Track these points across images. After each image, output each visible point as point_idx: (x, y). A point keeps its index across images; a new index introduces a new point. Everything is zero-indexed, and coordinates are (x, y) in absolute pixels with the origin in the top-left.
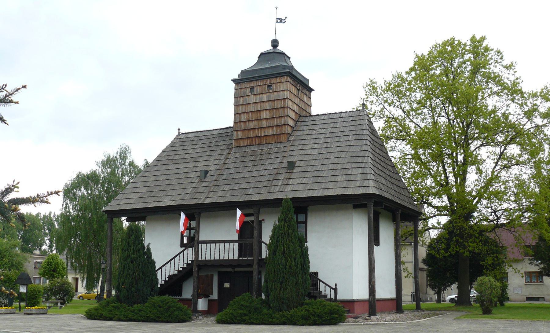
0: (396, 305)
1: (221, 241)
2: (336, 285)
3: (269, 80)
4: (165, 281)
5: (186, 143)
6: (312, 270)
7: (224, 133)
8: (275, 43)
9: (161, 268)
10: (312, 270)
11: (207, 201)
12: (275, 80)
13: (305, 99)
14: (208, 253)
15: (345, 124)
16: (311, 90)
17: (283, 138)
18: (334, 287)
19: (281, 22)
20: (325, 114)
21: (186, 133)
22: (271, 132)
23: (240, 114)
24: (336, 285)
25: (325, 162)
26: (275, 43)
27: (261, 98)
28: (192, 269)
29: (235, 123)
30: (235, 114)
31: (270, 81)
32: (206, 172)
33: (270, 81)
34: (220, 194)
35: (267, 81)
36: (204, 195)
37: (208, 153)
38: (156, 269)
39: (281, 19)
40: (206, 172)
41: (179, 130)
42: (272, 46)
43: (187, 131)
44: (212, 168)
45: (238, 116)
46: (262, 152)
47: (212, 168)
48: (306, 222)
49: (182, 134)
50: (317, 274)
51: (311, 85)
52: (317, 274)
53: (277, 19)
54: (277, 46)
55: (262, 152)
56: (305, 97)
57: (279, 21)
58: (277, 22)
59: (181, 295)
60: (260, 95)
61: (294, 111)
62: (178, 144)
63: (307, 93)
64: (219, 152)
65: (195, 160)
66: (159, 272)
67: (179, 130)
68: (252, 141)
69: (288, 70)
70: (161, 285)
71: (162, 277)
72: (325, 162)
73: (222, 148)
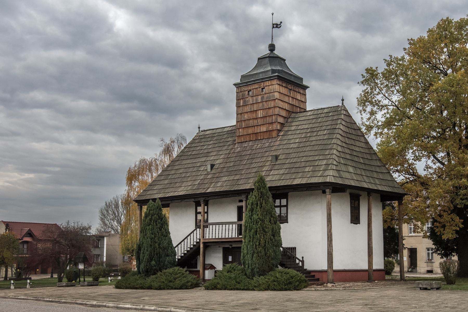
0: (368, 276)
1: (224, 222)
2: (303, 258)
3: (262, 84)
4: (181, 256)
5: (203, 140)
6: (285, 244)
7: (232, 132)
8: (272, 47)
9: (177, 246)
10: (285, 244)
11: (209, 191)
12: (267, 83)
13: (299, 97)
14: (213, 233)
15: (325, 119)
16: (305, 88)
17: (274, 134)
18: (301, 259)
19: (277, 27)
20: (312, 110)
21: (204, 131)
22: (264, 129)
23: (241, 114)
24: (303, 258)
25: (302, 154)
26: (272, 47)
27: (257, 100)
28: (200, 246)
29: (237, 122)
30: (237, 114)
31: (264, 84)
32: (277, 157)
33: (264, 84)
34: (219, 184)
35: (261, 84)
36: (207, 186)
37: (217, 149)
38: (174, 246)
39: (277, 24)
40: (277, 157)
41: (199, 128)
42: (270, 50)
43: (205, 129)
44: (218, 162)
45: (239, 115)
46: (257, 147)
47: (218, 162)
48: (286, 206)
49: (202, 131)
50: (293, 249)
51: (305, 83)
52: (293, 249)
53: (273, 24)
54: (274, 50)
55: (257, 147)
56: (299, 95)
57: (275, 26)
58: (273, 27)
59: (196, 268)
60: (256, 97)
61: (285, 109)
62: (197, 141)
63: (301, 91)
64: (226, 147)
65: (207, 154)
66: (176, 249)
67: (199, 128)
68: (250, 137)
69: (277, 74)
70: (178, 259)
71: (180, 252)
72: (302, 154)
73: (228, 144)
